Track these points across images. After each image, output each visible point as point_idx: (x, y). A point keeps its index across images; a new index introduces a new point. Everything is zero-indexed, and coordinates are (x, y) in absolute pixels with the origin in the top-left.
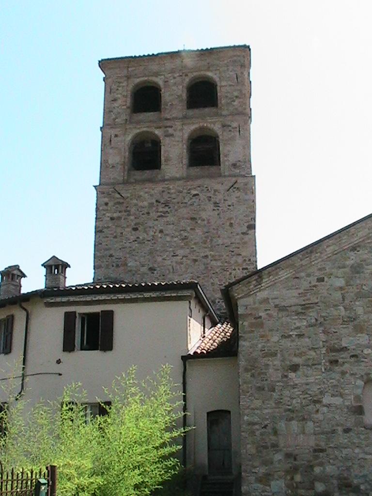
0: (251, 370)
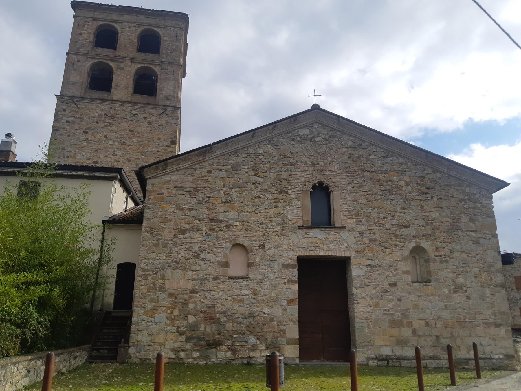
0: (151, 231)
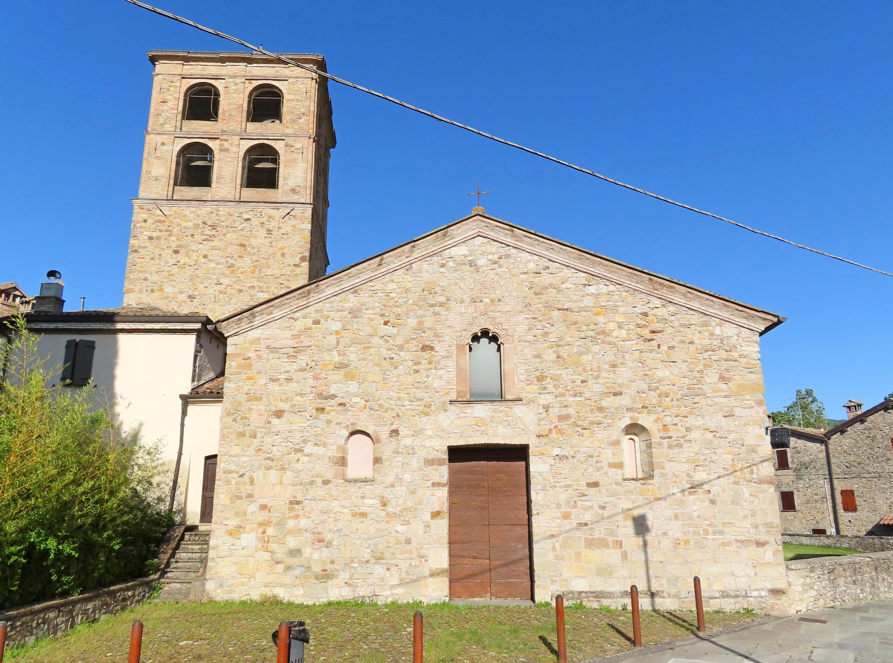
0: (233, 414)
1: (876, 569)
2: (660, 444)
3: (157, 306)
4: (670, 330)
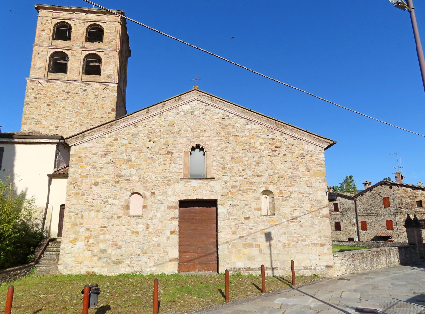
0: (73, 184)
1: (373, 256)
2: (278, 199)
3: (39, 131)
4: (284, 147)
